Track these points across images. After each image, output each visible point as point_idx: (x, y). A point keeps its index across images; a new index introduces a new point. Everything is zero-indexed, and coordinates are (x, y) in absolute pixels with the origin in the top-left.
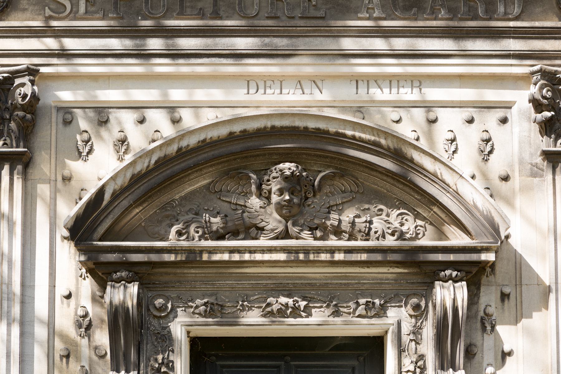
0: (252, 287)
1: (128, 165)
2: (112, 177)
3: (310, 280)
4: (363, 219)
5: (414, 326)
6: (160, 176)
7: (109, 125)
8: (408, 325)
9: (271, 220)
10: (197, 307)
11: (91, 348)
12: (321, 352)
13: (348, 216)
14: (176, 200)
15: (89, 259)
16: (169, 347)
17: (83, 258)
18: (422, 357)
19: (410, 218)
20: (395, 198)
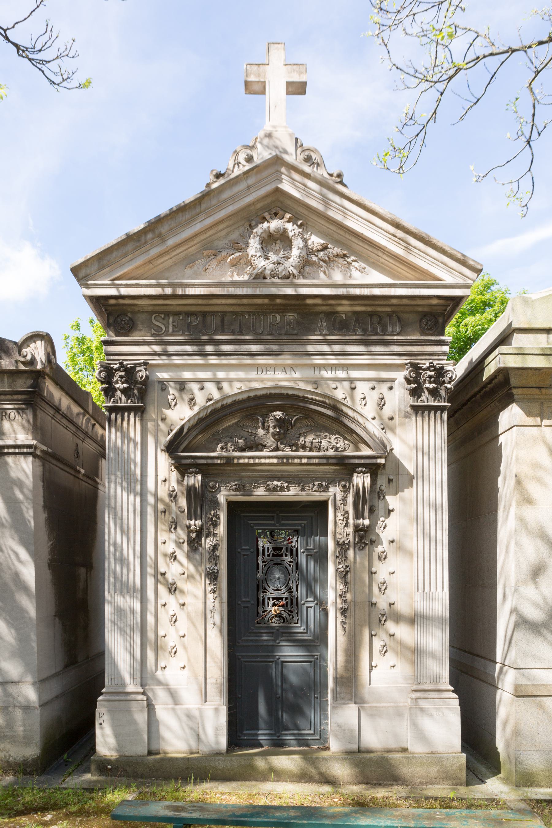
10: (231, 486)
13: (309, 438)
15: (176, 462)
17: (173, 462)
18: (347, 512)
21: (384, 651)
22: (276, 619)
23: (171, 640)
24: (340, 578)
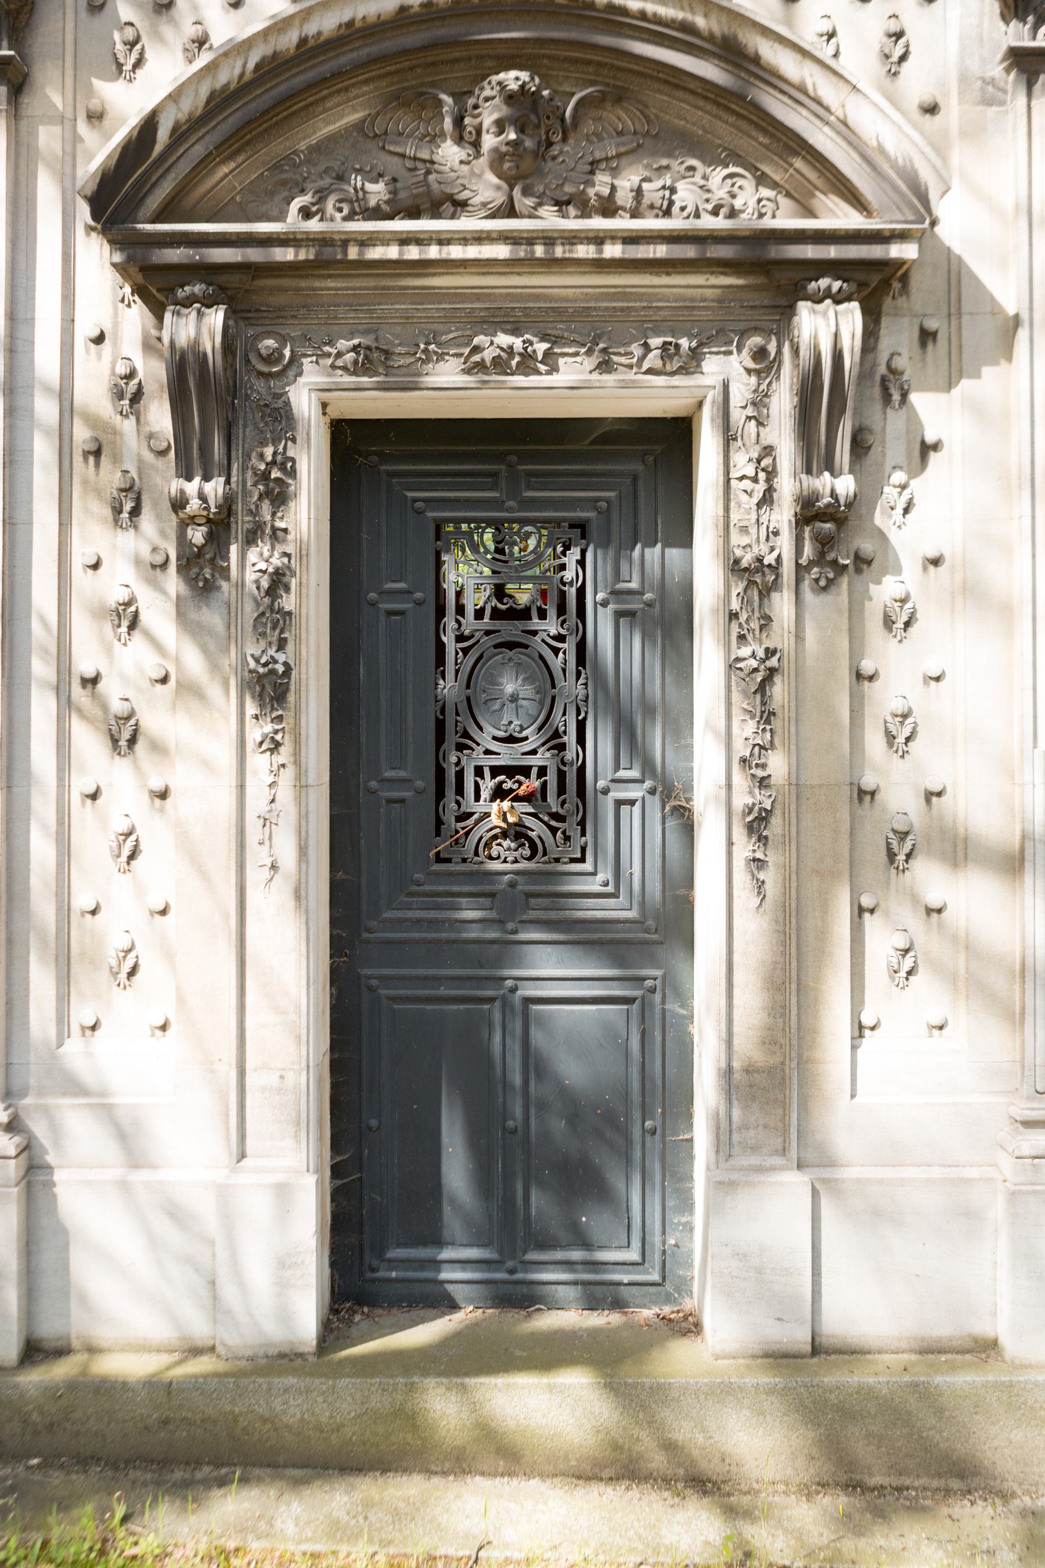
0: (445, 317)
1: (201, 70)
2: (170, 95)
3: (557, 301)
4: (659, 183)
5: (755, 391)
6: (266, 97)
7: (174, 11)
8: (743, 389)
9: (479, 186)
10: (339, 355)
11: (142, 437)
12: (573, 447)
13: (627, 182)
14: (302, 151)
15: (129, 259)
16: (286, 432)
17: (118, 258)
18: (768, 450)
19: (748, 183)
20: (720, 146)
21: (907, 966)
22: (506, 843)
23: (120, 925)
24: (744, 693)
